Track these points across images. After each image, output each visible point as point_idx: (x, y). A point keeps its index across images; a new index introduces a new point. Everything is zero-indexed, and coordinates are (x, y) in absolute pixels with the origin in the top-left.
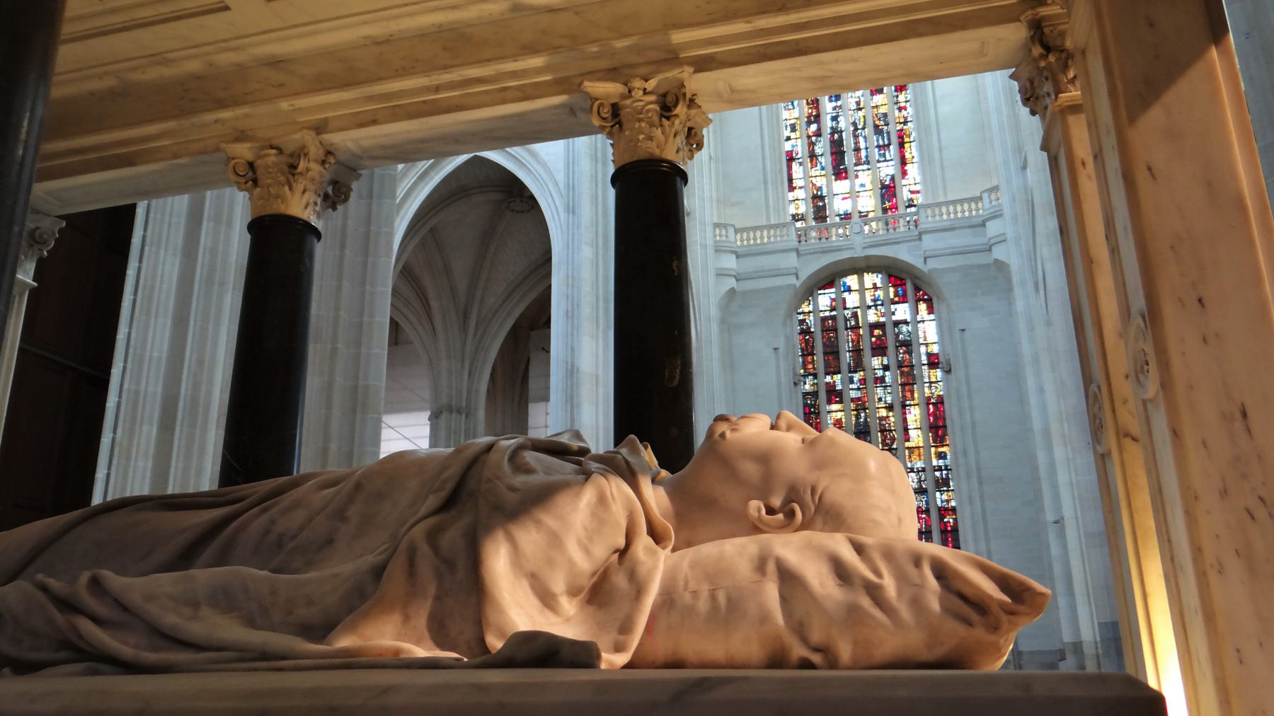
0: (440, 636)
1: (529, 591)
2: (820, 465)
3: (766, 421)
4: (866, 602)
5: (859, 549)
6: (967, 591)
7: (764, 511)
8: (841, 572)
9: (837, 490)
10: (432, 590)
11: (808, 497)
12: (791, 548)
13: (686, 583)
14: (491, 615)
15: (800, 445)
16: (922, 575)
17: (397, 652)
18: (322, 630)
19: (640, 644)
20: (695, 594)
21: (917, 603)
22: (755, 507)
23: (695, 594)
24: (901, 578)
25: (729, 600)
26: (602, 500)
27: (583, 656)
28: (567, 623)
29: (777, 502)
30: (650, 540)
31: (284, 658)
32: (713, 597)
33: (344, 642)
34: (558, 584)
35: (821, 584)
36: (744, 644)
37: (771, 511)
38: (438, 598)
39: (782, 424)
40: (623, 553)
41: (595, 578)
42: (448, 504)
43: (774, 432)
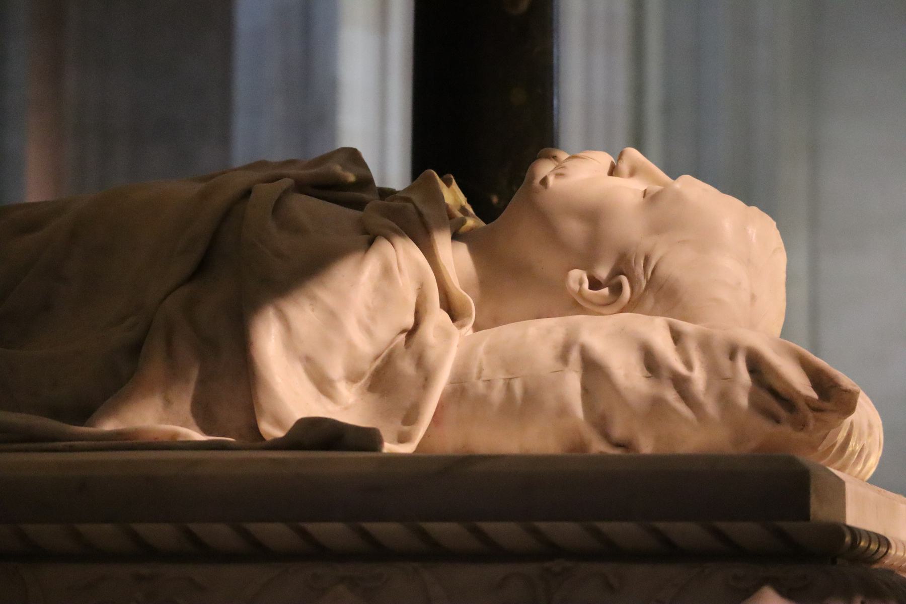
0: (204, 419)
1: (304, 376)
2: (658, 228)
3: (604, 159)
4: (671, 395)
5: (677, 337)
6: (778, 386)
7: (586, 285)
8: (651, 363)
9: (675, 261)
10: (194, 374)
11: (639, 270)
12: (656, 331)
13: (480, 371)
14: (264, 400)
15: (639, 198)
16: (734, 369)
17: (176, 434)
18: (85, 412)
19: (427, 435)
20: (489, 383)
21: (725, 398)
22: (577, 278)
23: (489, 383)
24: (713, 370)
25: (526, 391)
26: (387, 272)
27: (367, 439)
28: (349, 407)
29: (603, 273)
30: (445, 316)
31: (54, 440)
32: (509, 387)
33: (109, 426)
34: (336, 370)
35: (626, 376)
36: (535, 439)
37: (595, 284)
38: (202, 382)
39: (624, 166)
40: (411, 333)
41: (378, 362)
42: (201, 269)
43: (614, 180)
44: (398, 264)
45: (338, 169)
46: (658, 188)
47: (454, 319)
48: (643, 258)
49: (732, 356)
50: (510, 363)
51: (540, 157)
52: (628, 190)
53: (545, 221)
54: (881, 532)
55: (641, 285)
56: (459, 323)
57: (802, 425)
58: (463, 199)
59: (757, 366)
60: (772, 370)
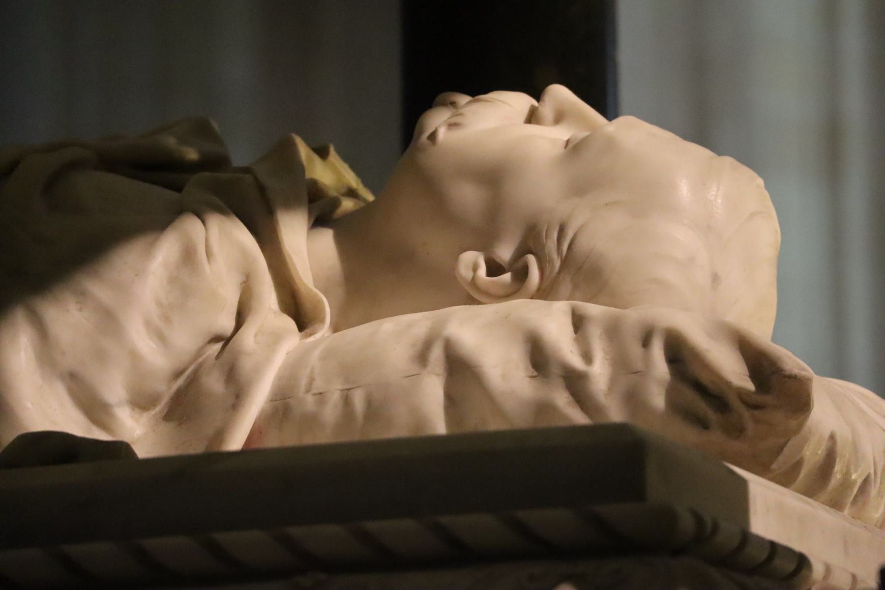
2: (580, 188)
5: (578, 322)
6: (705, 378)
7: (482, 271)
8: (539, 357)
9: (600, 230)
11: (551, 245)
12: (553, 321)
15: (559, 150)
16: (647, 359)
20: (321, 396)
22: (471, 263)
23: (321, 396)
24: (621, 364)
25: (369, 402)
26: (188, 256)
29: (505, 253)
32: (347, 401)
34: (114, 389)
37: (494, 269)
41: (181, 381)
43: (533, 129)
44: (207, 246)
45: (171, 142)
46: (585, 134)
47: (301, 327)
48: (557, 229)
49: (646, 342)
50: (350, 371)
51: (436, 105)
52: (550, 138)
53: (431, 189)
54: (797, 547)
55: (553, 266)
56: (307, 331)
57: (736, 430)
58: (352, 179)
59: (678, 352)
60: (697, 356)
